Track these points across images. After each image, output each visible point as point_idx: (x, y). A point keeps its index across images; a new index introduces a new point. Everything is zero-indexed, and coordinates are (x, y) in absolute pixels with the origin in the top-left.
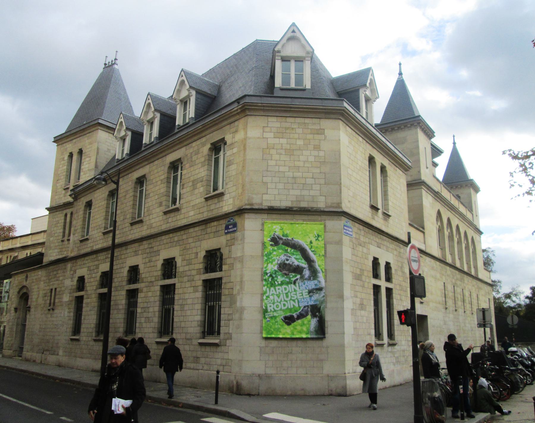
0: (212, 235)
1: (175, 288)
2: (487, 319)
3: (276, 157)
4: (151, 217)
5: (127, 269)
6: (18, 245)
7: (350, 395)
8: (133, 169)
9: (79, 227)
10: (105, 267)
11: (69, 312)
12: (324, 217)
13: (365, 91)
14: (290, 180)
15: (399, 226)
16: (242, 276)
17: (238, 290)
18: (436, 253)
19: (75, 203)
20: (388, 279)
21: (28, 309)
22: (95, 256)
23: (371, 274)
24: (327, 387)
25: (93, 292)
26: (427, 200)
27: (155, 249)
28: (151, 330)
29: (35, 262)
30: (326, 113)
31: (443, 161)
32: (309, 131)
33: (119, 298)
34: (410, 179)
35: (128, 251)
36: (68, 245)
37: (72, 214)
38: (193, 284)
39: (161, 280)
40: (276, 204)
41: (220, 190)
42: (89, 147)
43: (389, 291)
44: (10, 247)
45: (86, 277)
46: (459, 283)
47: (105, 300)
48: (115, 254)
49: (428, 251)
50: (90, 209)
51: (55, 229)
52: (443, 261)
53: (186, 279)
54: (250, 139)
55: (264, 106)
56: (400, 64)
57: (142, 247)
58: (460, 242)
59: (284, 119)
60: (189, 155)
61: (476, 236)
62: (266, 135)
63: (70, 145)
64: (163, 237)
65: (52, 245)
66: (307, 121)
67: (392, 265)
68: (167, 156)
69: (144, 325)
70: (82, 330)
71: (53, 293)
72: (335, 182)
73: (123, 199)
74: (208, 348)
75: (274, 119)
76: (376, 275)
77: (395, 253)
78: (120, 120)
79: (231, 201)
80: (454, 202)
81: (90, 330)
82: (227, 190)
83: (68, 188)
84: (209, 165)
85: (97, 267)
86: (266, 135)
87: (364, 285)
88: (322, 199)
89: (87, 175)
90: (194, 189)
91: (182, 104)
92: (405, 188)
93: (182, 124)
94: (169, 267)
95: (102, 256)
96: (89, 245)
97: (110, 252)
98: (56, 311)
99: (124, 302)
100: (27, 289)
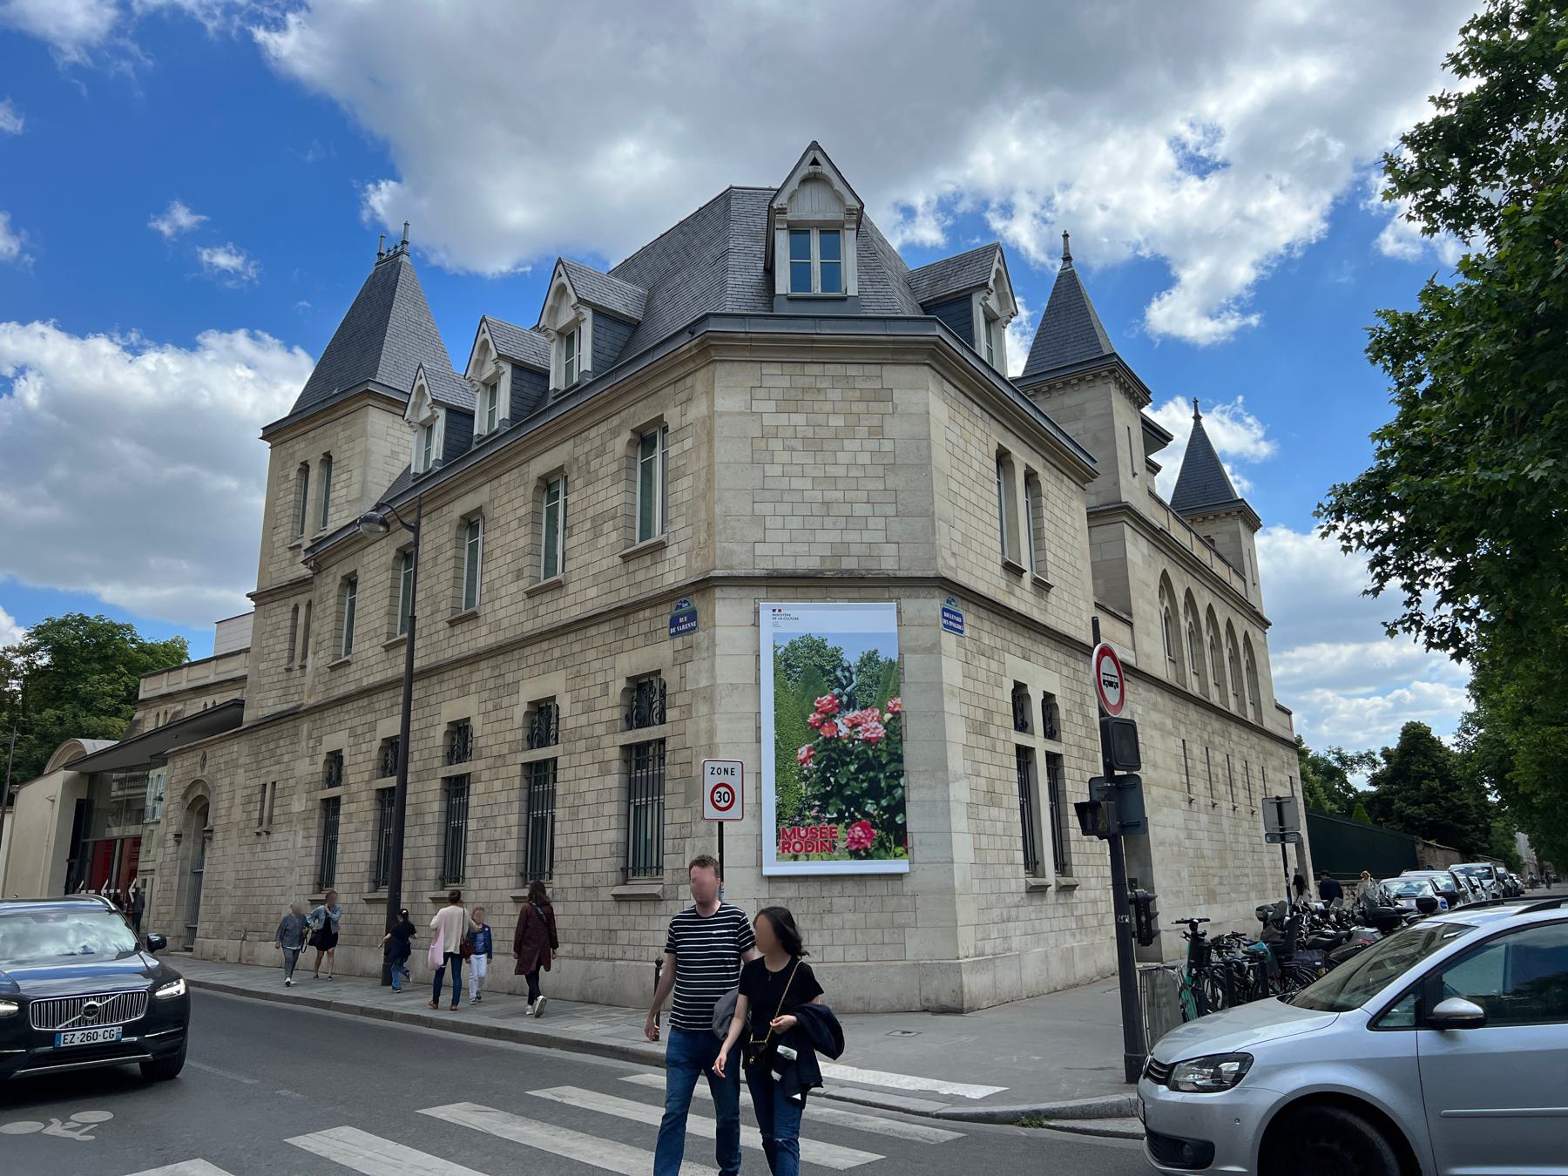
0: (640, 641)
1: (555, 768)
2: (1288, 823)
3: (784, 457)
4: (497, 604)
5: (443, 728)
6: (184, 685)
7: (971, 1010)
8: (453, 495)
9: (327, 636)
10: (390, 726)
11: (307, 838)
12: (896, 592)
13: (985, 299)
14: (817, 510)
15: (1071, 611)
16: (711, 733)
18: (1161, 670)
19: (317, 580)
20: (1051, 733)
21: (206, 836)
22: (364, 702)
23: (1010, 722)
26: (1137, 550)
27: (509, 678)
29: (224, 722)
30: (895, 351)
31: (1171, 463)
32: (857, 393)
33: (426, 799)
34: (1094, 501)
37: (309, 605)
38: (599, 755)
40: (786, 565)
41: (657, 536)
43: (1053, 760)
44: (164, 690)
46: (1217, 740)
47: (392, 804)
48: (415, 696)
49: (1142, 666)
50: (353, 592)
51: (271, 642)
52: (1177, 693)
54: (721, 415)
55: (751, 340)
56: (1066, 236)
57: (477, 676)
58: (1216, 646)
60: (582, 458)
61: (1255, 633)
62: (758, 406)
64: (527, 651)
66: (852, 370)
67: (1058, 701)
69: (485, 859)
70: (337, 878)
71: (268, 792)
72: (921, 515)
73: (429, 565)
74: (635, 907)
76: (1022, 725)
77: (1065, 671)
78: (418, 383)
79: (682, 561)
80: (1205, 556)
81: (357, 878)
83: (299, 546)
84: (630, 480)
85: (372, 727)
86: (758, 406)
87: (994, 746)
88: (891, 549)
89: (345, 513)
90: (596, 537)
92: (1082, 522)
93: (563, 388)
94: (542, 720)
98: (275, 837)
99: (436, 806)
100: (205, 787)
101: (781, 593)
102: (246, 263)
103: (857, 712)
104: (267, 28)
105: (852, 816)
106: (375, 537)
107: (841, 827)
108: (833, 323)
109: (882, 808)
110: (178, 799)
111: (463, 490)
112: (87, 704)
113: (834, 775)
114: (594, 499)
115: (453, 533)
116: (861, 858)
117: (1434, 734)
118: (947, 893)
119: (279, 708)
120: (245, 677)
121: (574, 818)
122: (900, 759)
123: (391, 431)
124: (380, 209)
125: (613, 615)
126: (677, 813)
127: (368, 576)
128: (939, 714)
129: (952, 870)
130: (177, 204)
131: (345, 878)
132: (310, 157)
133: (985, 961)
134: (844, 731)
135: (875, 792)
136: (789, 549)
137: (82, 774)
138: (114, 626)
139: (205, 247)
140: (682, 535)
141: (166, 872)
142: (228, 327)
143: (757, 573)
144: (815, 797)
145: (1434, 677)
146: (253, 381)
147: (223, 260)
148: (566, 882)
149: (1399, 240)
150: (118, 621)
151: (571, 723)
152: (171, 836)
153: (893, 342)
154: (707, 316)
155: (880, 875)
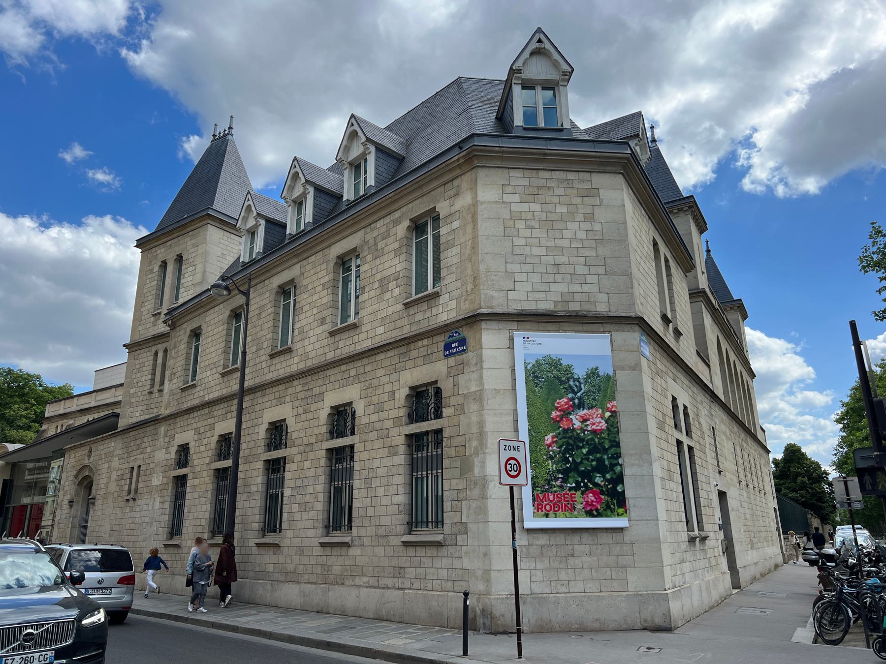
0: (420, 361)
3: (526, 232)
4: (306, 342)
5: (265, 426)
6: (75, 408)
8: (273, 272)
10: (228, 426)
11: (163, 502)
12: (608, 327)
16: (481, 424)
17: (476, 448)
19: (173, 334)
21: (90, 501)
24: (637, 615)
25: (205, 467)
27: (316, 391)
28: (309, 524)
30: (601, 164)
32: (575, 192)
33: (252, 476)
35: (266, 399)
36: (160, 399)
37: (166, 351)
38: (388, 442)
39: (327, 440)
40: (530, 307)
42: (193, 250)
44: (62, 411)
45: (191, 445)
47: (226, 481)
51: (139, 375)
53: (373, 435)
54: (482, 203)
55: (503, 152)
57: (290, 391)
59: (534, 173)
63: (163, 250)
64: (330, 372)
65: (133, 400)
66: (571, 176)
68: (333, 247)
69: (298, 516)
70: (184, 530)
73: (255, 319)
74: (421, 551)
75: (519, 173)
79: (453, 304)
82: (443, 288)
83: (160, 313)
84: (409, 253)
85: (212, 427)
86: (507, 198)
88: (603, 297)
89: (191, 292)
90: (383, 293)
91: (351, 169)
92: (687, 297)
94: (342, 419)
95: (219, 410)
96: (197, 395)
97: (236, 402)
98: (139, 502)
100: (91, 470)
101: (528, 325)
102: (114, 179)
103: (585, 411)
104: (129, 49)
105: (586, 485)
106: (220, 299)
107: (579, 493)
108: (559, 142)
109: (607, 480)
110: (72, 478)
111: (279, 269)
112: (11, 422)
113: (572, 455)
114: (381, 267)
115: (273, 297)
116: (594, 516)
117: (803, 450)
118: (655, 542)
119: (143, 418)
120: (120, 402)
121: (368, 486)
122: (618, 445)
123: (222, 241)
124: (189, 150)
125: (398, 344)
126: (454, 482)
127: (209, 329)
128: (643, 413)
129: (657, 525)
130: (76, 144)
131: (190, 529)
132: (153, 122)
133: (680, 591)
134: (577, 424)
135: (601, 468)
136: (531, 296)
137: (7, 463)
138: (29, 376)
139: (91, 169)
140: (452, 287)
141: (62, 526)
142: (100, 214)
143: (511, 311)
144: (559, 472)
145: (776, 421)
146: (114, 244)
147: (101, 177)
148: (363, 532)
149: (753, 182)
150: (32, 372)
151: (365, 420)
152: (66, 502)
153: (599, 157)
154: (473, 135)
155: (594, 529)
